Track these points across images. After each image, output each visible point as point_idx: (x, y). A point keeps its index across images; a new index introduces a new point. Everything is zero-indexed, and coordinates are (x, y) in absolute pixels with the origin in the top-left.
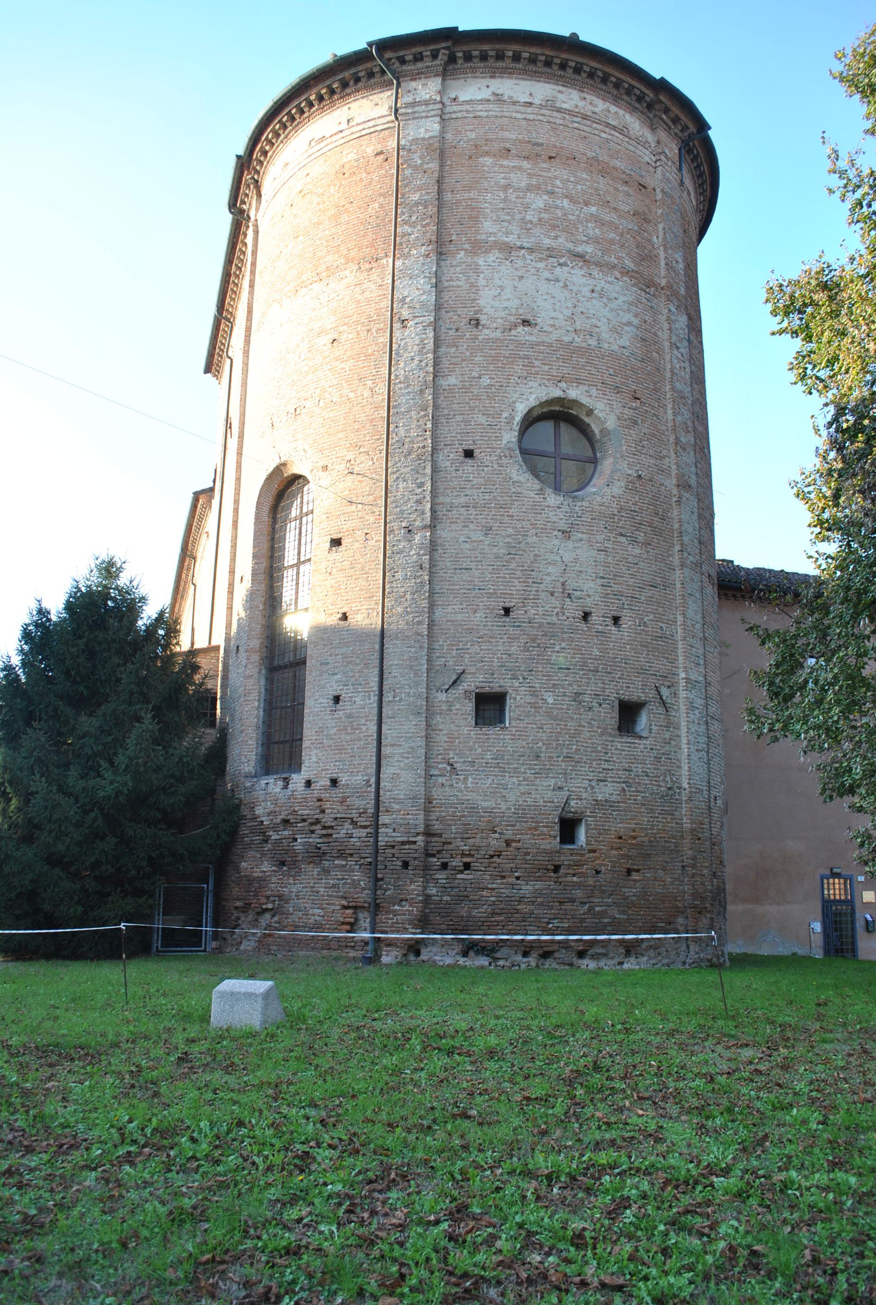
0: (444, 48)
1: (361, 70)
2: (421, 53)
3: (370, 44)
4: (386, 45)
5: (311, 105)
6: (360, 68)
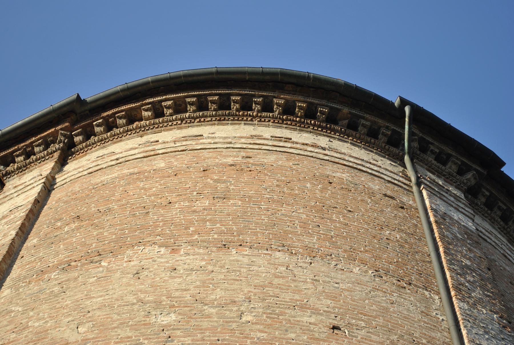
0: (475, 170)
1: (368, 119)
2: (449, 156)
3: (404, 102)
4: (422, 118)
5: (267, 107)
6: (367, 116)
